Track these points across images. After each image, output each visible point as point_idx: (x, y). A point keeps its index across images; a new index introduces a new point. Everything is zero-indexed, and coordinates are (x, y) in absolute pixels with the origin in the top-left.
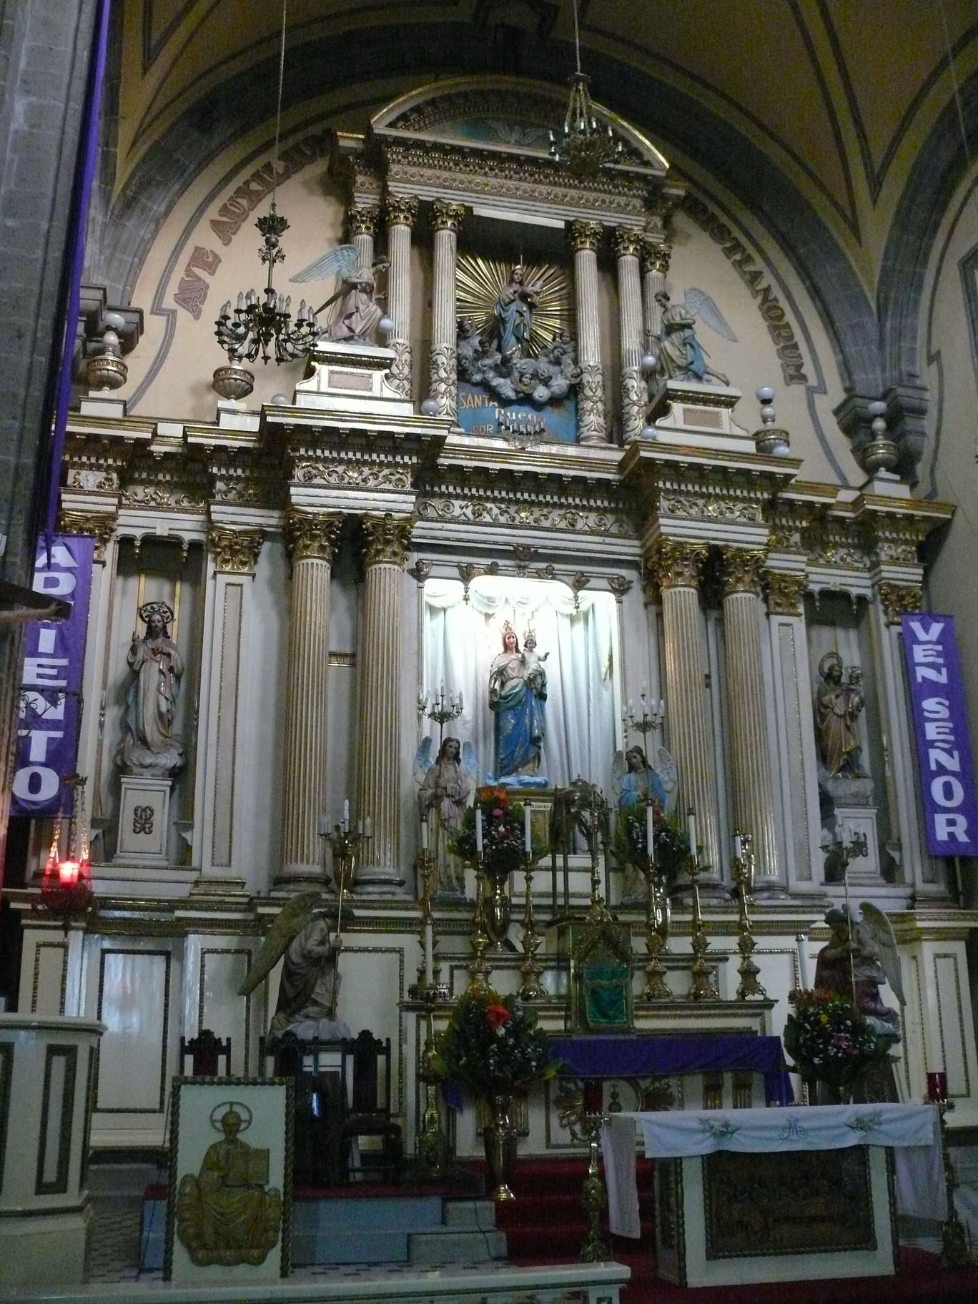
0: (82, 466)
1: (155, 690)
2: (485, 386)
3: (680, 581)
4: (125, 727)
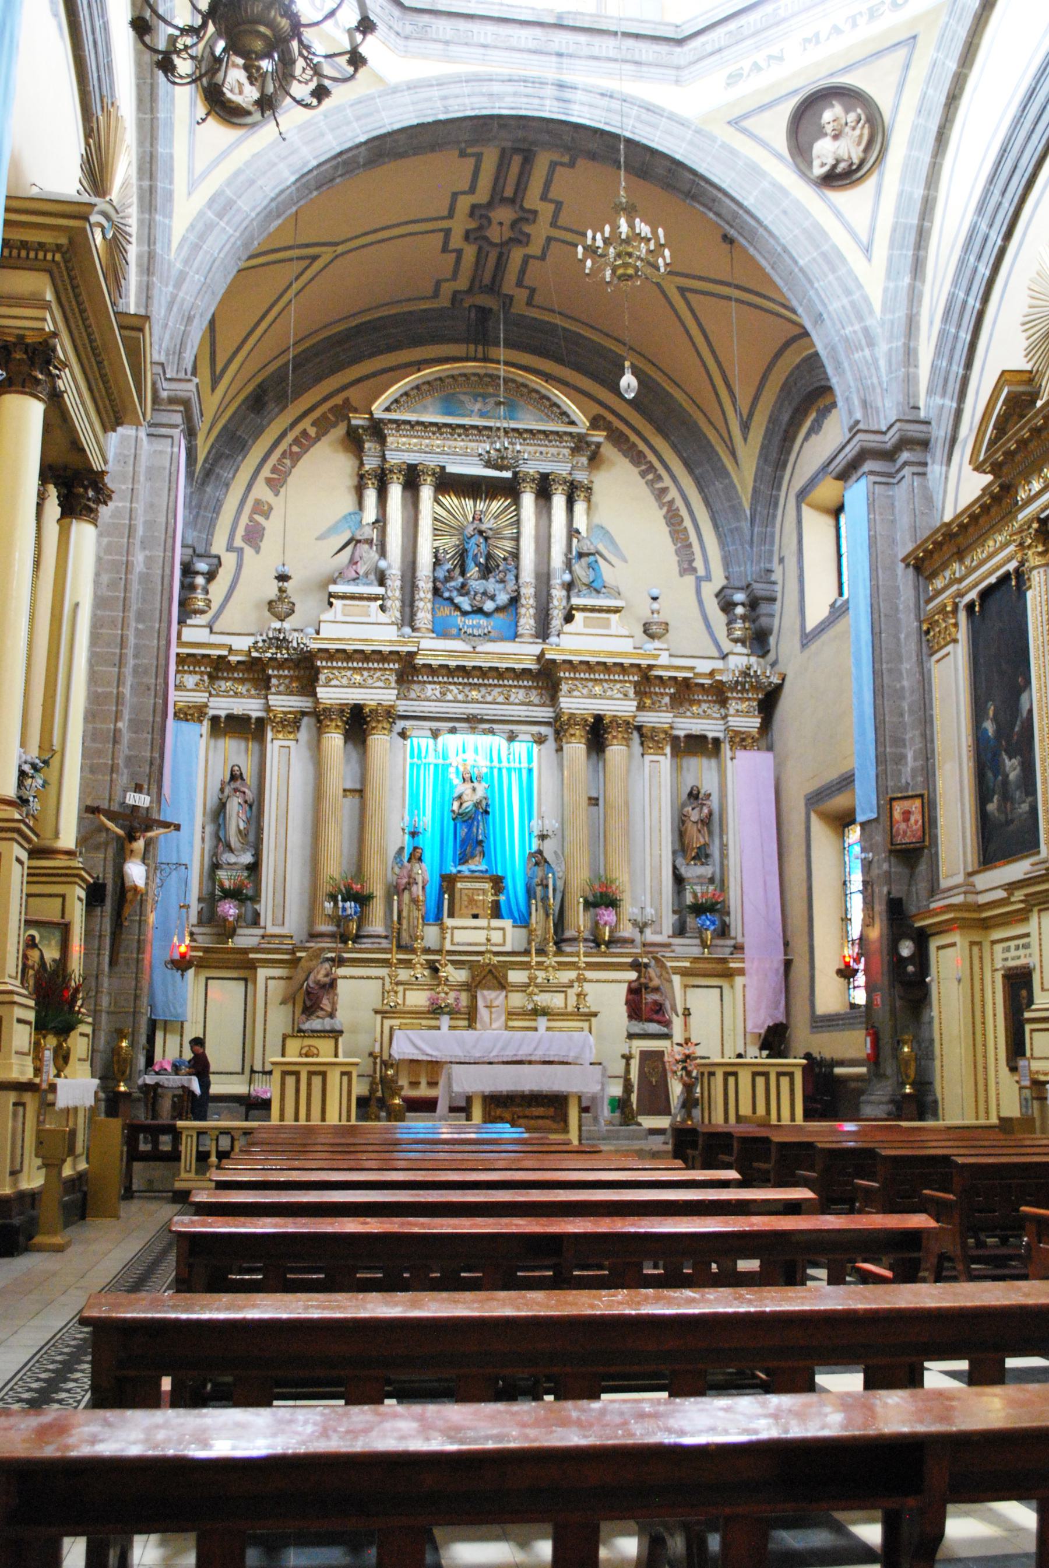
0: (185, 672)
1: (236, 816)
2: (450, 600)
3: (573, 739)
4: (218, 839)
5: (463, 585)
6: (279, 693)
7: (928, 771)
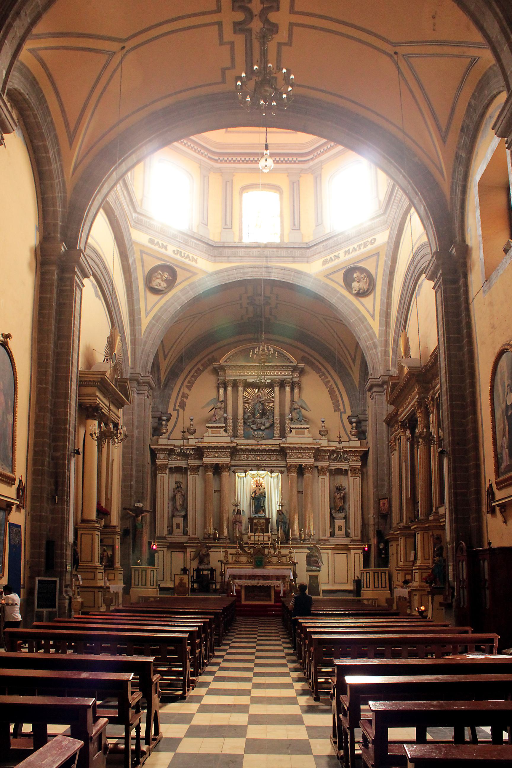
2: (249, 425)
5: (253, 421)
6: (191, 460)
7: (390, 490)
